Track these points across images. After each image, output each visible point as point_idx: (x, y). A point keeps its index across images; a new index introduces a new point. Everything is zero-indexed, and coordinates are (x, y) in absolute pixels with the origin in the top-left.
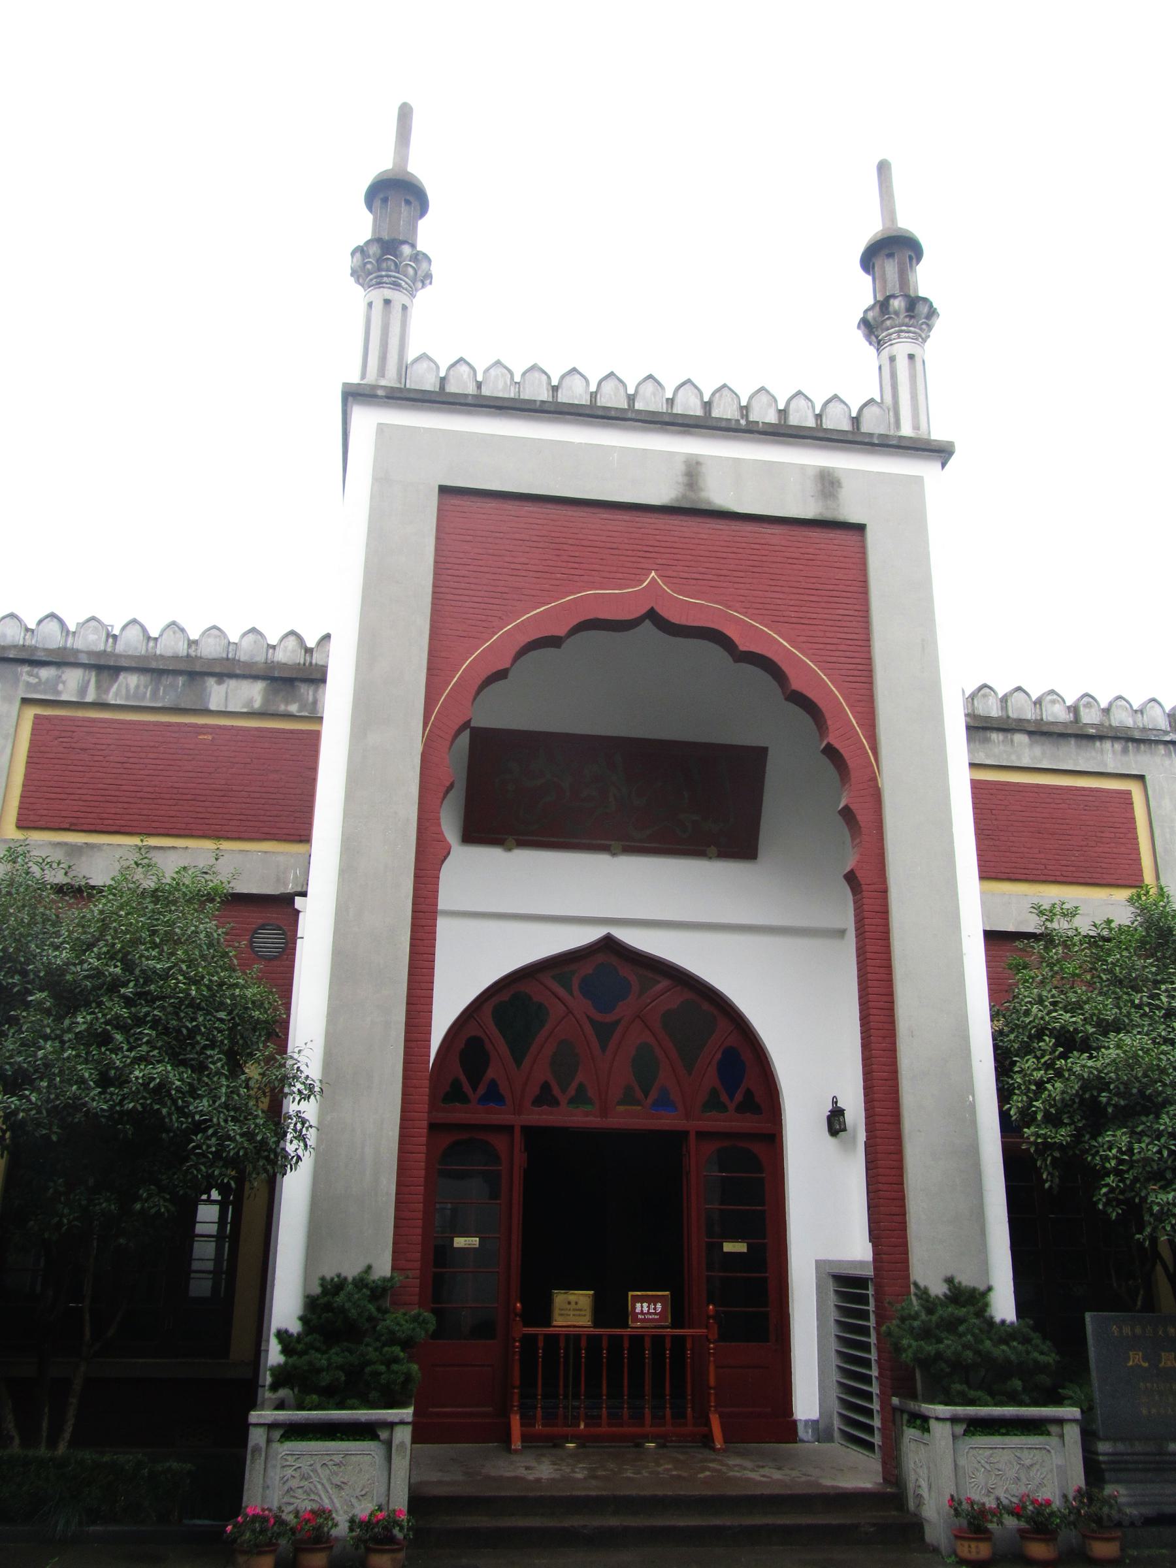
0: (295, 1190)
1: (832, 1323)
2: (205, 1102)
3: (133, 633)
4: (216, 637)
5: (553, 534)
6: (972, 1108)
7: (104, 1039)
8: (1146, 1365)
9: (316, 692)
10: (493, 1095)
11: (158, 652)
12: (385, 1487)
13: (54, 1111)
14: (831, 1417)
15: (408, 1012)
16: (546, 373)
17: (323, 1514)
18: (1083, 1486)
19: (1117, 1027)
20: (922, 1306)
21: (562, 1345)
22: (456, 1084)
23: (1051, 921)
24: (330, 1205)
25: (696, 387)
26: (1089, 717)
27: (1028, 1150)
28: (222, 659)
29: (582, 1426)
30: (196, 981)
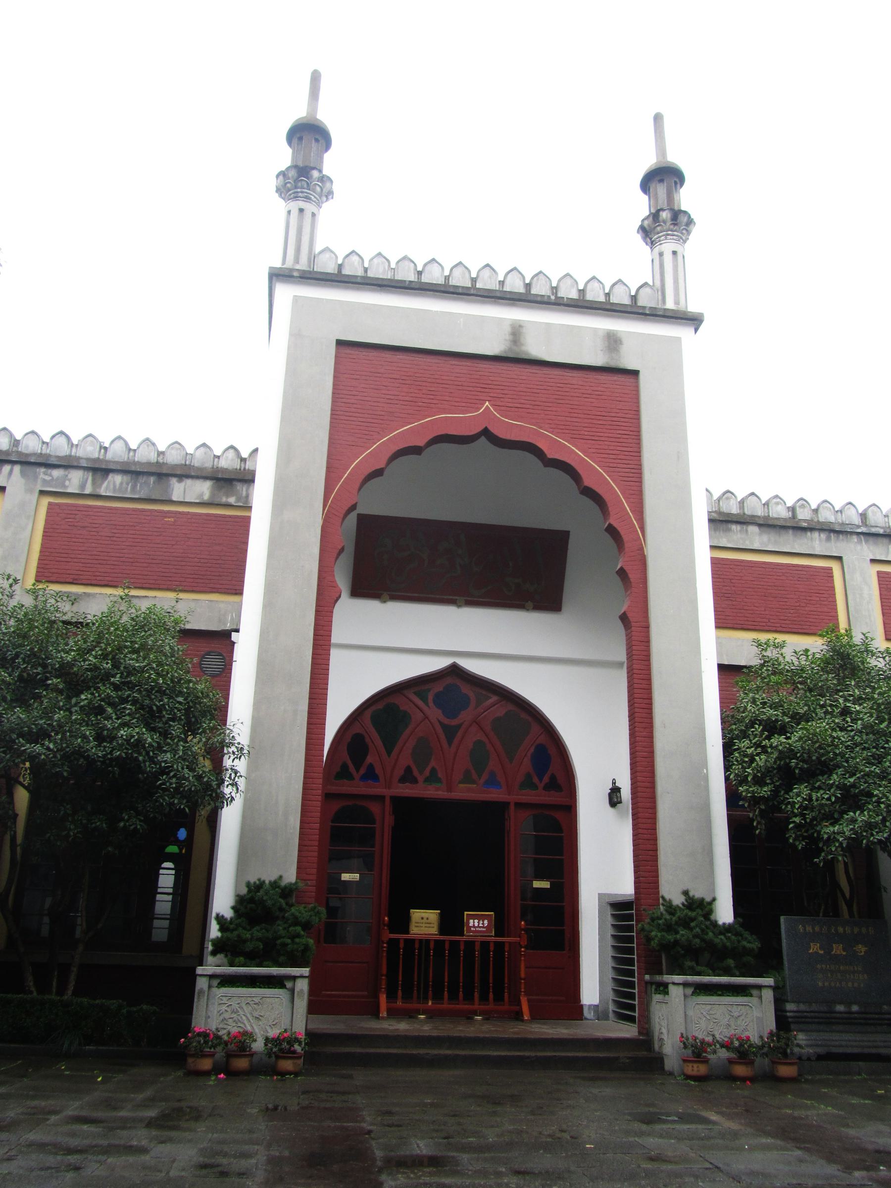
0: (230, 819)
1: (609, 937)
2: (168, 755)
3: (119, 445)
4: (177, 449)
5: (417, 375)
6: (706, 778)
7: (100, 711)
8: (822, 952)
10: (371, 775)
11: (136, 459)
12: (289, 1019)
13: (66, 757)
14: (607, 1004)
15: (310, 704)
16: (413, 262)
17: (250, 1035)
18: (775, 1031)
19: (806, 717)
20: (666, 911)
21: (417, 946)
22: (345, 767)
24: (255, 828)
25: (520, 273)
26: (803, 515)
28: (182, 465)
29: (430, 1003)
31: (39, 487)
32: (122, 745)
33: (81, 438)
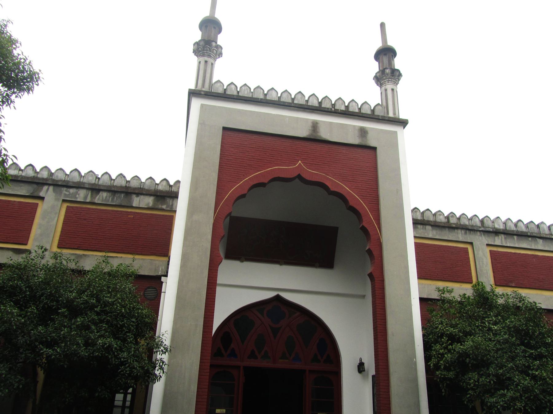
0: (158, 389)
2: (125, 354)
3: (106, 177)
7: (88, 328)
9: (173, 200)
15: (204, 321)
23: (443, 294)
27: (437, 380)
30: (123, 306)
31: (63, 198)
32: (100, 348)
33: (86, 172)
